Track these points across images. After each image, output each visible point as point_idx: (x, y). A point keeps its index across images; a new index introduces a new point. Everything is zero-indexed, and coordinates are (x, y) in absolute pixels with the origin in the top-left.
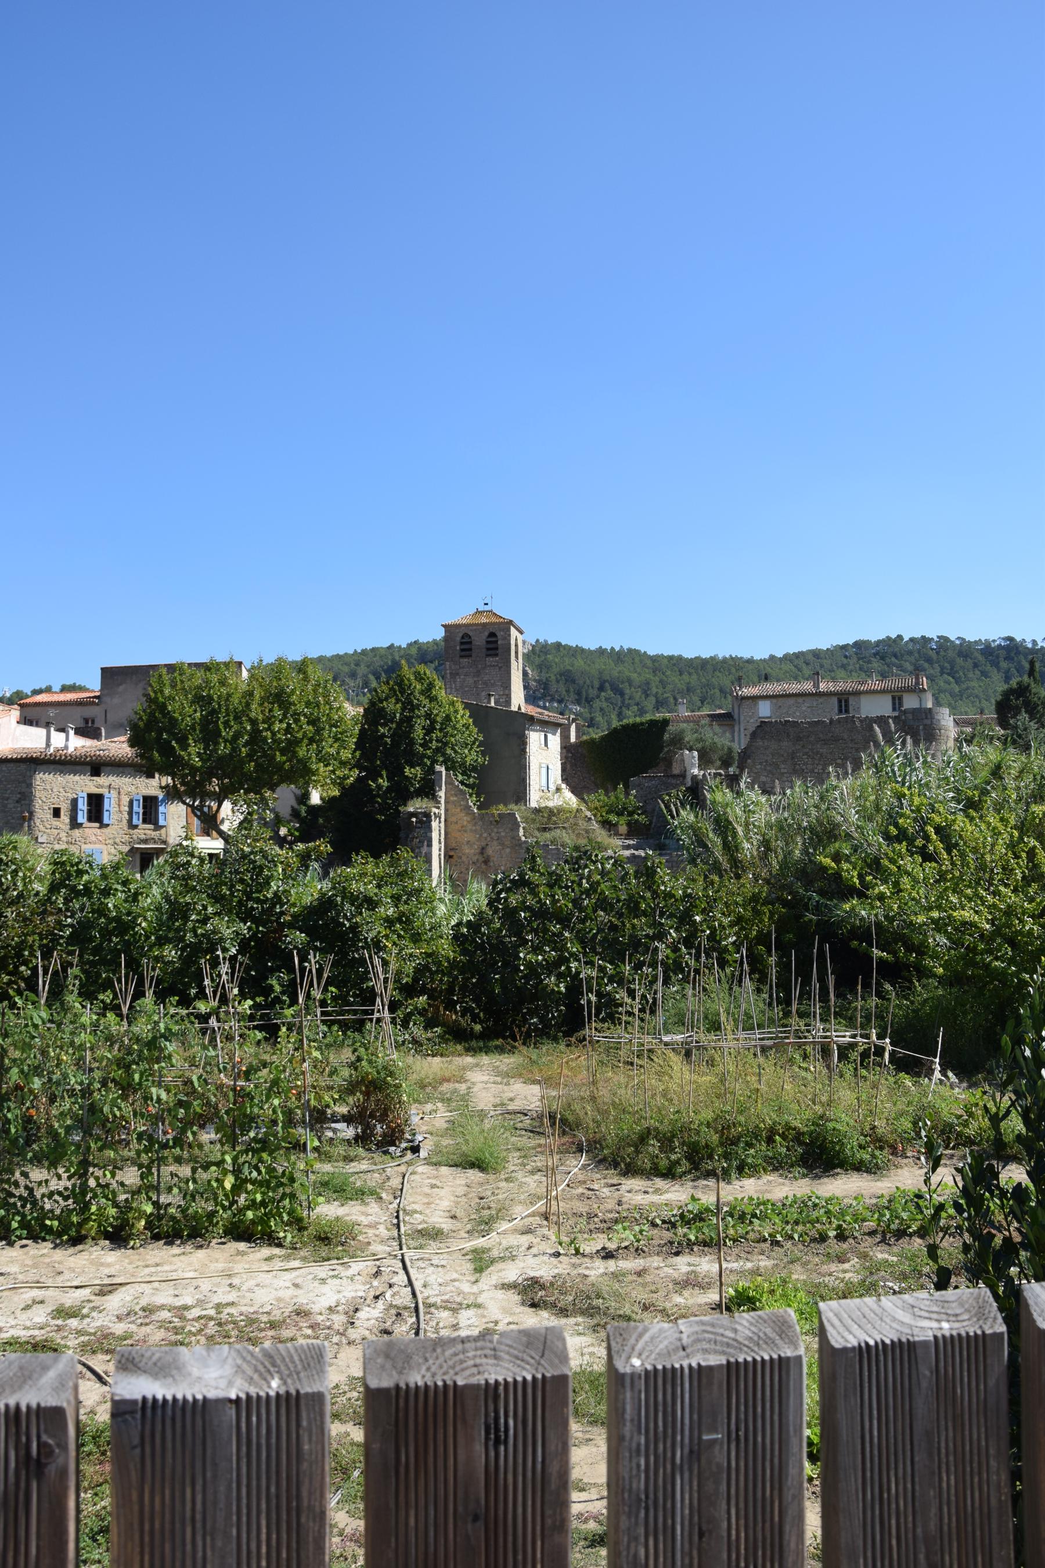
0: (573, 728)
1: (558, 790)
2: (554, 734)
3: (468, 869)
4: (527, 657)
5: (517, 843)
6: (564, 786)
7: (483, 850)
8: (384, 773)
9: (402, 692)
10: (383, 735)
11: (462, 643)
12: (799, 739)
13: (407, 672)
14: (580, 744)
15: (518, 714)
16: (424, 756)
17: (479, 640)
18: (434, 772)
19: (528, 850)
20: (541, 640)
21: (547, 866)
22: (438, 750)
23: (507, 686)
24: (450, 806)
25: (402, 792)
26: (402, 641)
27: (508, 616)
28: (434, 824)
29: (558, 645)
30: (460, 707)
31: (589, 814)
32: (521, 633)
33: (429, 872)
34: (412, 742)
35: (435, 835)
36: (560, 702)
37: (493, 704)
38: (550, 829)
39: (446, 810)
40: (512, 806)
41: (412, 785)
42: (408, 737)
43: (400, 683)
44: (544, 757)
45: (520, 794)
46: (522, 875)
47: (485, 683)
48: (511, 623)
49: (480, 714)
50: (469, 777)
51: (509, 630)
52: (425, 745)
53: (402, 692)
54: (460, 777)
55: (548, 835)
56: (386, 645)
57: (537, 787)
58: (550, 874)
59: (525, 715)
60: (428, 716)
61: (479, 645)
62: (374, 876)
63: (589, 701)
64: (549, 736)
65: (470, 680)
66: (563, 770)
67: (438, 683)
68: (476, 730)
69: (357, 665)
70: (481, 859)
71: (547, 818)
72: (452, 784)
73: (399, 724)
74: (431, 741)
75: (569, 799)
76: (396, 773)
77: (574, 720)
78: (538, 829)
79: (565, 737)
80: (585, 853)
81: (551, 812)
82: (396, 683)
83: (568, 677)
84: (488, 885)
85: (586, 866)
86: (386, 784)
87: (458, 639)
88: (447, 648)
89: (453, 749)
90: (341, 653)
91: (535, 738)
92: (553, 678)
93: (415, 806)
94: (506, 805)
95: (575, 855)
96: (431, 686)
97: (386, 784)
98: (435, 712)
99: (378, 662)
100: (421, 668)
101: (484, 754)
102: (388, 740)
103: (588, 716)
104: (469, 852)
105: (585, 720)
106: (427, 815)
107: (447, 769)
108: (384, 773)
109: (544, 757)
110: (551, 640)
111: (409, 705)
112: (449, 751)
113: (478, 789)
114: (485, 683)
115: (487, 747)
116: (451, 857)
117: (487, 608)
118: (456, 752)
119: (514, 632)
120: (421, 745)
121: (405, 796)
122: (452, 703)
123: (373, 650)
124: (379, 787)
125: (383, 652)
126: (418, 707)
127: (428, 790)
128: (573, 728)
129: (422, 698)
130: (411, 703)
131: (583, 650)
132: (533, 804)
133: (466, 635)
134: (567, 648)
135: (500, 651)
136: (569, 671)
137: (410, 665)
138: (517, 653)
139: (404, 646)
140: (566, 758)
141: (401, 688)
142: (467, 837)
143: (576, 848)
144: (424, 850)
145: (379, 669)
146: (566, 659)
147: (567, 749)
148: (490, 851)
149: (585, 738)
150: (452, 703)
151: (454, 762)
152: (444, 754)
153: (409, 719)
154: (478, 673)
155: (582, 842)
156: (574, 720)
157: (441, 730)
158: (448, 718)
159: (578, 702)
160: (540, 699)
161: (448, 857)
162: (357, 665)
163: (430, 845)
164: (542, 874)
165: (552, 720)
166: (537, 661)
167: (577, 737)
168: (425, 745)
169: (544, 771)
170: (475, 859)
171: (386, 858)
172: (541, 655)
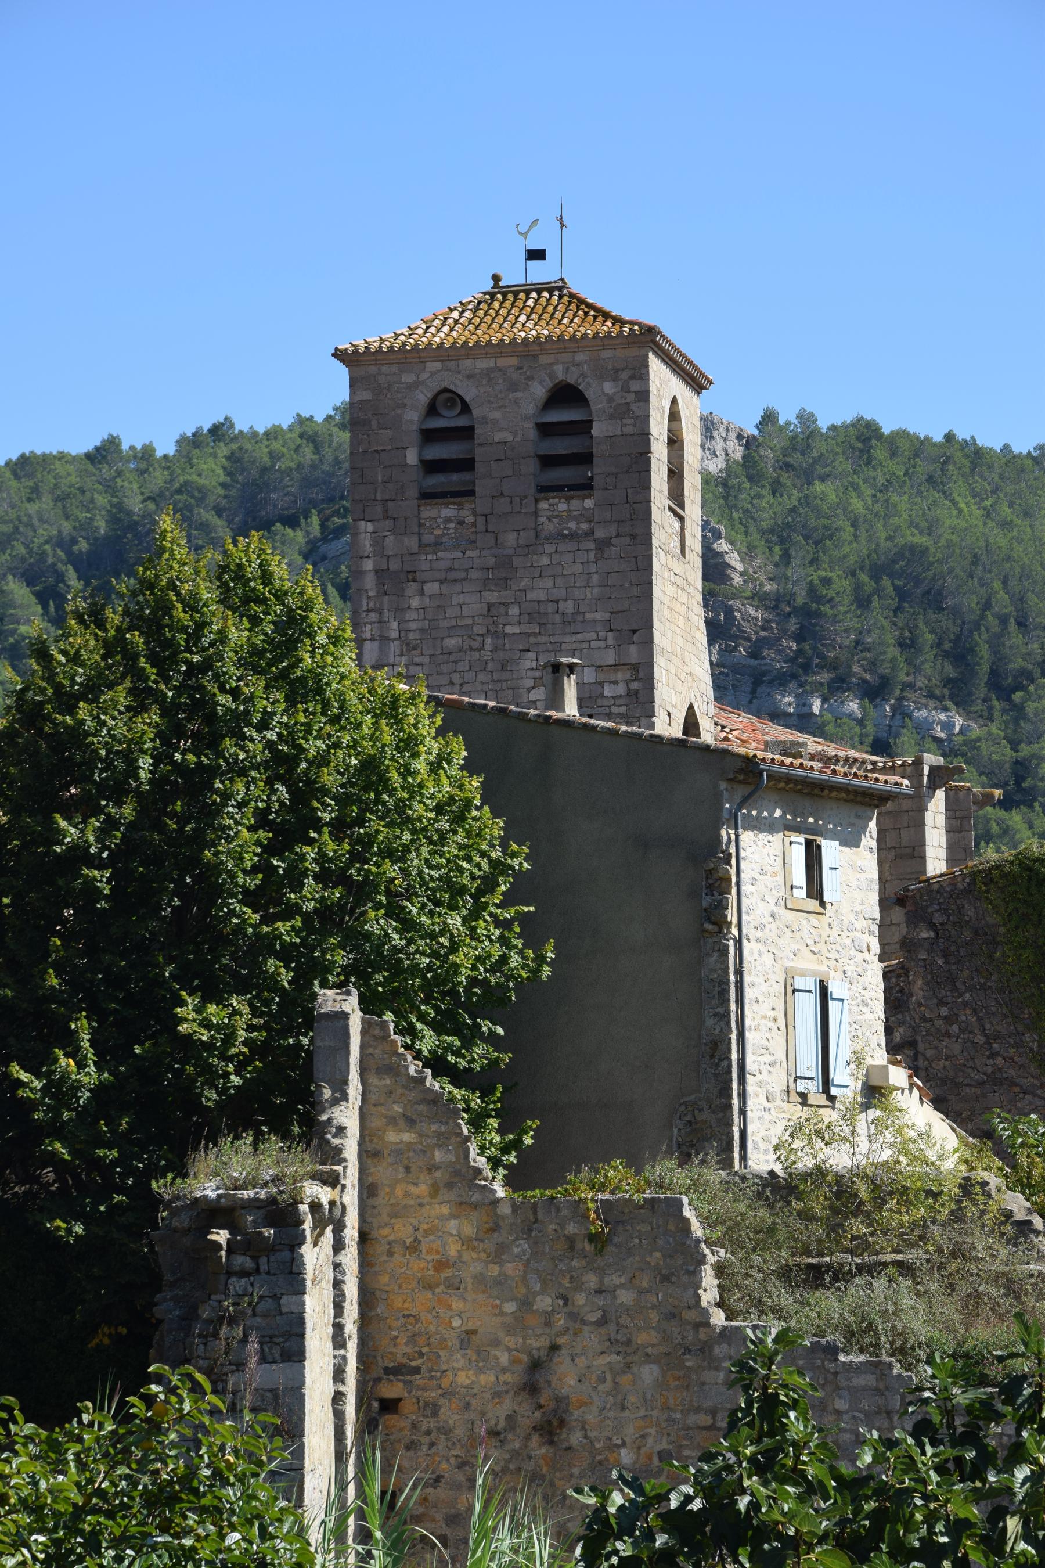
0: (936, 812)
1: (874, 1093)
2: (851, 841)
3: (466, 1464)
4: (721, 490)
5: (691, 1343)
6: (898, 1076)
7: (535, 1373)
8: (82, 1028)
9: (164, 658)
10: (79, 855)
11: (429, 436)
13: (187, 568)
14: (969, 884)
15: (686, 747)
16: (265, 945)
17: (508, 421)
18: (310, 1020)
19: (744, 1374)
20: (787, 415)
21: (832, 1451)
22: (326, 918)
23: (635, 626)
24: (382, 1173)
25: (168, 1114)
26: (157, 428)
27: (632, 306)
28: (314, 1256)
29: (863, 437)
30: (423, 721)
31: (1018, 1204)
32: (697, 382)
33: (290, 1481)
34: (210, 886)
35: (316, 1307)
36: (873, 692)
37: (571, 709)
38: (840, 1275)
39: (368, 1191)
40: (666, 1168)
41: (212, 1077)
42: (195, 861)
43: (153, 619)
44: (807, 939)
45: (706, 1119)
46: (719, 1490)
47: (534, 615)
48: (649, 338)
49: (511, 753)
50: (470, 1036)
51: (641, 373)
52: (268, 897)
53: (164, 658)
54: (429, 1041)
55: (831, 1304)
56: (81, 442)
57: (778, 1081)
58: (853, 1487)
59: (717, 757)
60: (281, 764)
61: (507, 439)
62: (34, 1507)
63: (1005, 686)
64: (831, 850)
65: (468, 603)
66: (896, 1002)
67: (327, 617)
68: (496, 828)
70: (529, 1416)
71: (826, 1221)
72: (393, 1069)
73: (153, 804)
74: (295, 878)
75: (929, 1135)
76: (135, 1018)
77: (939, 777)
78: (785, 1274)
79: (900, 853)
80: (1012, 1386)
81: (845, 1198)
82: (134, 620)
83: (908, 581)
84: (563, 1540)
85: (1017, 1454)
86: (91, 1076)
87: (413, 417)
88: (362, 456)
89: (394, 911)
91: (763, 859)
92: (842, 584)
93: (224, 1172)
94: (636, 1164)
95: (961, 1396)
96: (293, 629)
97: (91, 1076)
98: (314, 746)
99: (47, 525)
100: (249, 550)
101: (533, 932)
102: (101, 878)
103: (1004, 753)
104: (474, 1381)
105: (989, 773)
106: (282, 1215)
107: (368, 1005)
108: (82, 1028)
109: (807, 939)
110: (832, 413)
111: (197, 720)
112: (376, 922)
113: (509, 1093)
114: (534, 615)
115: (546, 904)
116: (389, 1406)
117: (540, 273)
118: (407, 925)
119: (663, 383)
120: (250, 898)
121: (183, 1133)
122: (391, 709)
124: (60, 1091)
126: (236, 725)
127: (284, 1100)
128: (936, 812)
129: (254, 685)
130: (203, 707)
131: (976, 456)
132: (762, 1160)
133: (446, 399)
134: (908, 447)
135: (599, 469)
136: (917, 553)
137: (200, 536)
138: (676, 474)
139: (166, 447)
140: (907, 945)
141: (156, 643)
142: (464, 1312)
143: (969, 1366)
144: (256, 1374)
145: (55, 556)
146: (901, 501)
147: (904, 899)
148: (566, 1378)
149: (991, 854)
150: (391, 709)
151: (396, 970)
152: (354, 938)
153: (197, 782)
154: (502, 572)
155: (992, 1334)
156: (939, 777)
157: (339, 828)
158: (371, 775)
159: (957, 693)
160: (782, 681)
161: (378, 1409)
163: (296, 1355)
164: (812, 1489)
165: (841, 776)
166: (769, 509)
167: (955, 851)
168: (268, 897)
169: (807, 1006)
170: (498, 1413)
171: (95, 1424)
172: (783, 472)
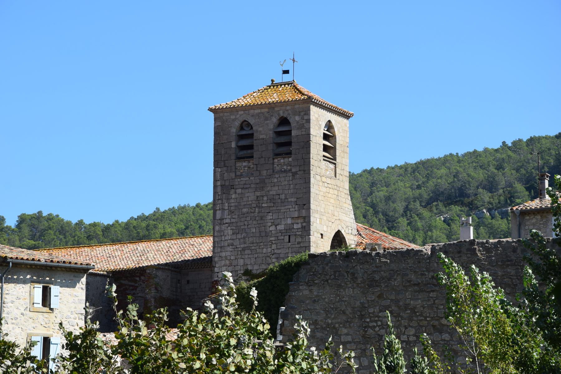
10: (554, 260)
12: (372, 283)
17: (265, 131)
47: (272, 200)
64: (55, 290)
65: (251, 196)
69: (499, 167)
87: (234, 130)
90: (480, 149)
117: (287, 78)
123: (532, 141)
125: (546, 144)
135: (293, 148)
154: (261, 185)
162: (499, 167)
